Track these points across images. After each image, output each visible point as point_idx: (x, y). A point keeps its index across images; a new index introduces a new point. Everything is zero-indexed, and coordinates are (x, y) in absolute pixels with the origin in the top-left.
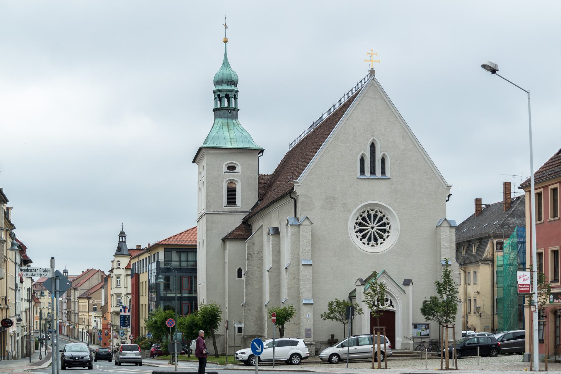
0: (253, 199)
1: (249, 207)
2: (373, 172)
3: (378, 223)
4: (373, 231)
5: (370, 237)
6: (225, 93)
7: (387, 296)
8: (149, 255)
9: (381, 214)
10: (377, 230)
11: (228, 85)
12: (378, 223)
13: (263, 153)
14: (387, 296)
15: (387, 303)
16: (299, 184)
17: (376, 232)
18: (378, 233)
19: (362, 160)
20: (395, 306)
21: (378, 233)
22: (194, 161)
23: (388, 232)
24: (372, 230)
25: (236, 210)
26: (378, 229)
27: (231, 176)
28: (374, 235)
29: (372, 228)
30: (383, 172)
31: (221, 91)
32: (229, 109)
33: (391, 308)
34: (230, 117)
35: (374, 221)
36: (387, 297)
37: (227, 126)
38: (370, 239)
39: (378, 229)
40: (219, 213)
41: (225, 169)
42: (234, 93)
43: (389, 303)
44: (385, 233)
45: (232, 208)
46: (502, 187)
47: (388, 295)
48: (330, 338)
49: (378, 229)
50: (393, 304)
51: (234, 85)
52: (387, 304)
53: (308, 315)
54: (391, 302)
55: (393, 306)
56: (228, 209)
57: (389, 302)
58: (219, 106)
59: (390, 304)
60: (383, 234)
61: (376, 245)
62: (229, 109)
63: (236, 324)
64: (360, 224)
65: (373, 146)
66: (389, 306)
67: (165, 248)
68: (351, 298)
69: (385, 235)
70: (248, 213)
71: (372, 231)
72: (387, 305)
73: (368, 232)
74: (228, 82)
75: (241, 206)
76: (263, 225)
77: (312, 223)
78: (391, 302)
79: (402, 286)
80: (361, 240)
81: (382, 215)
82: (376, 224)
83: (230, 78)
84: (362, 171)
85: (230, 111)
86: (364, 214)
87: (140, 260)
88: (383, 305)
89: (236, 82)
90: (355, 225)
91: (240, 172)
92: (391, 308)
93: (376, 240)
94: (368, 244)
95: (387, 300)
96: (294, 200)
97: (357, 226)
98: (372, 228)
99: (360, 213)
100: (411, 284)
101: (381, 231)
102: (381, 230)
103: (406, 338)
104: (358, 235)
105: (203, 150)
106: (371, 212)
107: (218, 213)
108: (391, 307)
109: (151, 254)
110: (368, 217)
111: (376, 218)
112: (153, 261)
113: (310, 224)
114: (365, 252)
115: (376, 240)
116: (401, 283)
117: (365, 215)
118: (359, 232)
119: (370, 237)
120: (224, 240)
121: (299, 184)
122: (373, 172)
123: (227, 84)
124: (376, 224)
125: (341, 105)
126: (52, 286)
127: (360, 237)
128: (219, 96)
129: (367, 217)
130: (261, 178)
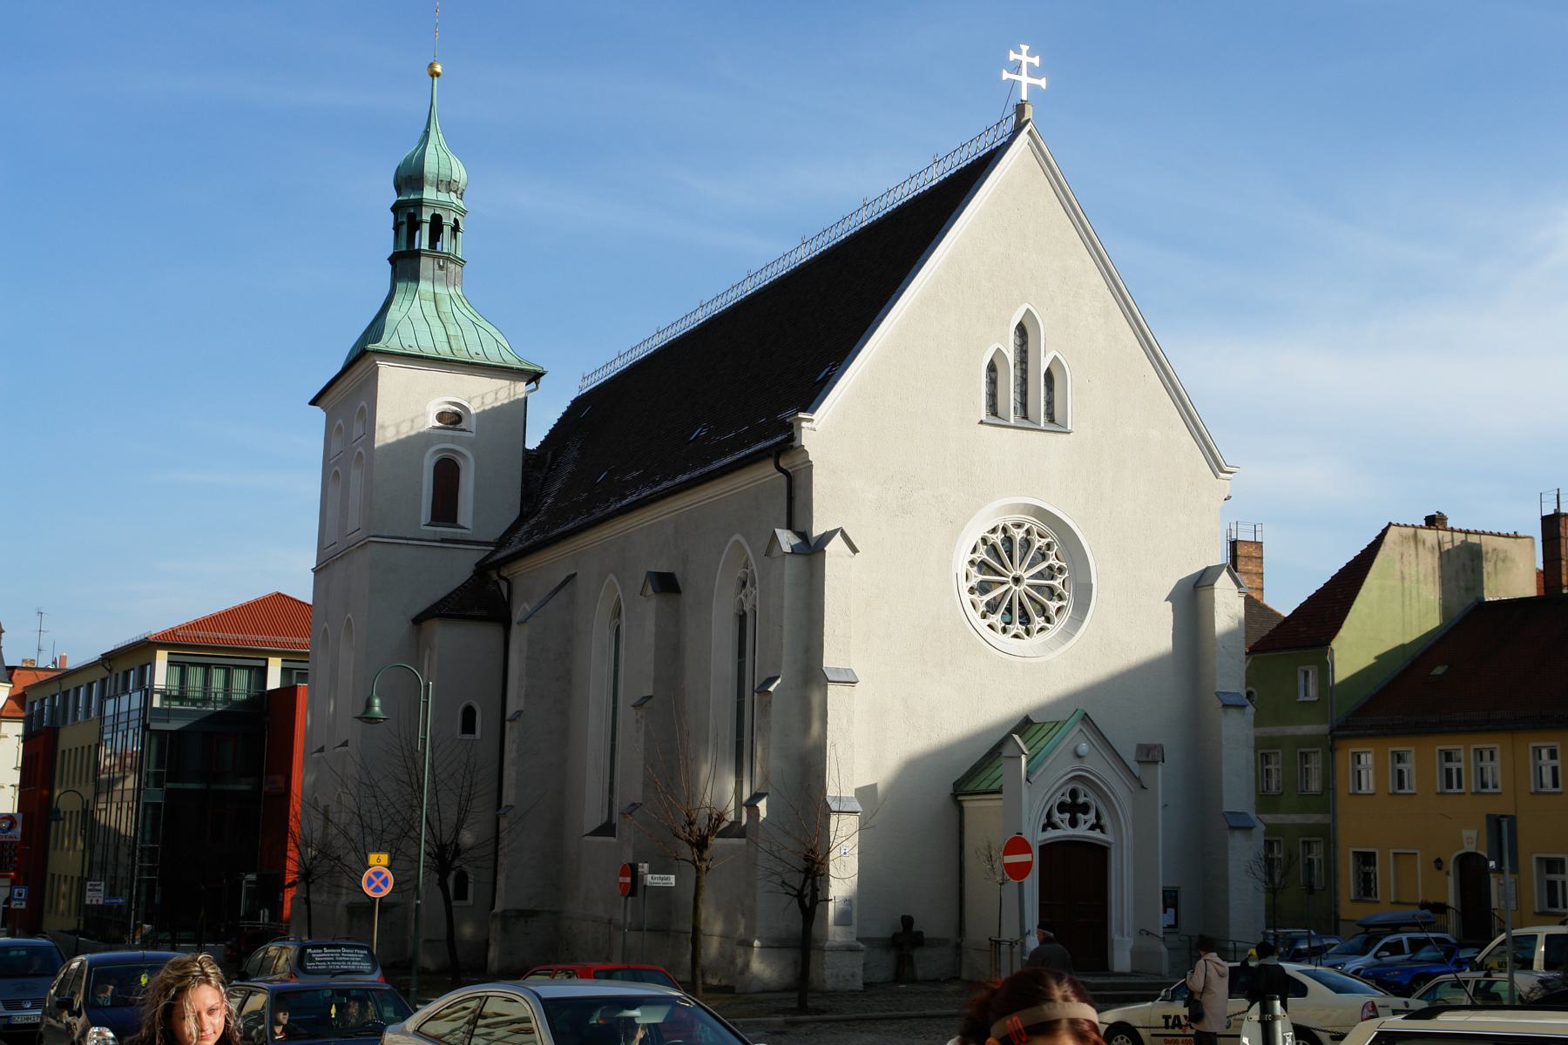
0: (508, 509)
1: (495, 531)
5: (1009, 610)
8: (106, 674)
9: (1043, 540)
13: (539, 385)
14: (1085, 796)
15: (1086, 817)
20: (1109, 828)
22: (314, 402)
24: (1014, 587)
25: (459, 537)
29: (1017, 580)
30: (1051, 417)
33: (1096, 834)
34: (440, 280)
36: (1087, 799)
37: (433, 304)
39: (1030, 586)
40: (405, 542)
43: (1091, 817)
45: (447, 531)
47: (1090, 793)
48: (900, 930)
50: (1102, 822)
51: (455, 192)
52: (1085, 822)
54: (1098, 817)
56: (435, 532)
58: (404, 249)
60: (1045, 601)
63: (649, 876)
64: (983, 566)
66: (1092, 828)
67: (169, 653)
68: (960, 798)
70: (492, 548)
72: (1088, 825)
74: (442, 181)
75: (470, 527)
76: (572, 577)
77: (854, 550)
78: (1098, 817)
85: (441, 264)
86: (1015, 530)
87: (64, 689)
88: (1073, 823)
89: (460, 186)
91: (473, 429)
92: (1097, 834)
95: (1085, 809)
96: (784, 476)
98: (1017, 580)
99: (1009, 520)
102: (1038, 588)
103: (1148, 934)
107: (410, 542)
108: (1098, 830)
109: (115, 671)
110: (1003, 545)
112: (112, 692)
116: (1130, 758)
117: (1018, 535)
119: (1009, 610)
120: (418, 621)
123: (437, 187)
125: (887, 209)
126: (1060, 538)
130: (526, 452)
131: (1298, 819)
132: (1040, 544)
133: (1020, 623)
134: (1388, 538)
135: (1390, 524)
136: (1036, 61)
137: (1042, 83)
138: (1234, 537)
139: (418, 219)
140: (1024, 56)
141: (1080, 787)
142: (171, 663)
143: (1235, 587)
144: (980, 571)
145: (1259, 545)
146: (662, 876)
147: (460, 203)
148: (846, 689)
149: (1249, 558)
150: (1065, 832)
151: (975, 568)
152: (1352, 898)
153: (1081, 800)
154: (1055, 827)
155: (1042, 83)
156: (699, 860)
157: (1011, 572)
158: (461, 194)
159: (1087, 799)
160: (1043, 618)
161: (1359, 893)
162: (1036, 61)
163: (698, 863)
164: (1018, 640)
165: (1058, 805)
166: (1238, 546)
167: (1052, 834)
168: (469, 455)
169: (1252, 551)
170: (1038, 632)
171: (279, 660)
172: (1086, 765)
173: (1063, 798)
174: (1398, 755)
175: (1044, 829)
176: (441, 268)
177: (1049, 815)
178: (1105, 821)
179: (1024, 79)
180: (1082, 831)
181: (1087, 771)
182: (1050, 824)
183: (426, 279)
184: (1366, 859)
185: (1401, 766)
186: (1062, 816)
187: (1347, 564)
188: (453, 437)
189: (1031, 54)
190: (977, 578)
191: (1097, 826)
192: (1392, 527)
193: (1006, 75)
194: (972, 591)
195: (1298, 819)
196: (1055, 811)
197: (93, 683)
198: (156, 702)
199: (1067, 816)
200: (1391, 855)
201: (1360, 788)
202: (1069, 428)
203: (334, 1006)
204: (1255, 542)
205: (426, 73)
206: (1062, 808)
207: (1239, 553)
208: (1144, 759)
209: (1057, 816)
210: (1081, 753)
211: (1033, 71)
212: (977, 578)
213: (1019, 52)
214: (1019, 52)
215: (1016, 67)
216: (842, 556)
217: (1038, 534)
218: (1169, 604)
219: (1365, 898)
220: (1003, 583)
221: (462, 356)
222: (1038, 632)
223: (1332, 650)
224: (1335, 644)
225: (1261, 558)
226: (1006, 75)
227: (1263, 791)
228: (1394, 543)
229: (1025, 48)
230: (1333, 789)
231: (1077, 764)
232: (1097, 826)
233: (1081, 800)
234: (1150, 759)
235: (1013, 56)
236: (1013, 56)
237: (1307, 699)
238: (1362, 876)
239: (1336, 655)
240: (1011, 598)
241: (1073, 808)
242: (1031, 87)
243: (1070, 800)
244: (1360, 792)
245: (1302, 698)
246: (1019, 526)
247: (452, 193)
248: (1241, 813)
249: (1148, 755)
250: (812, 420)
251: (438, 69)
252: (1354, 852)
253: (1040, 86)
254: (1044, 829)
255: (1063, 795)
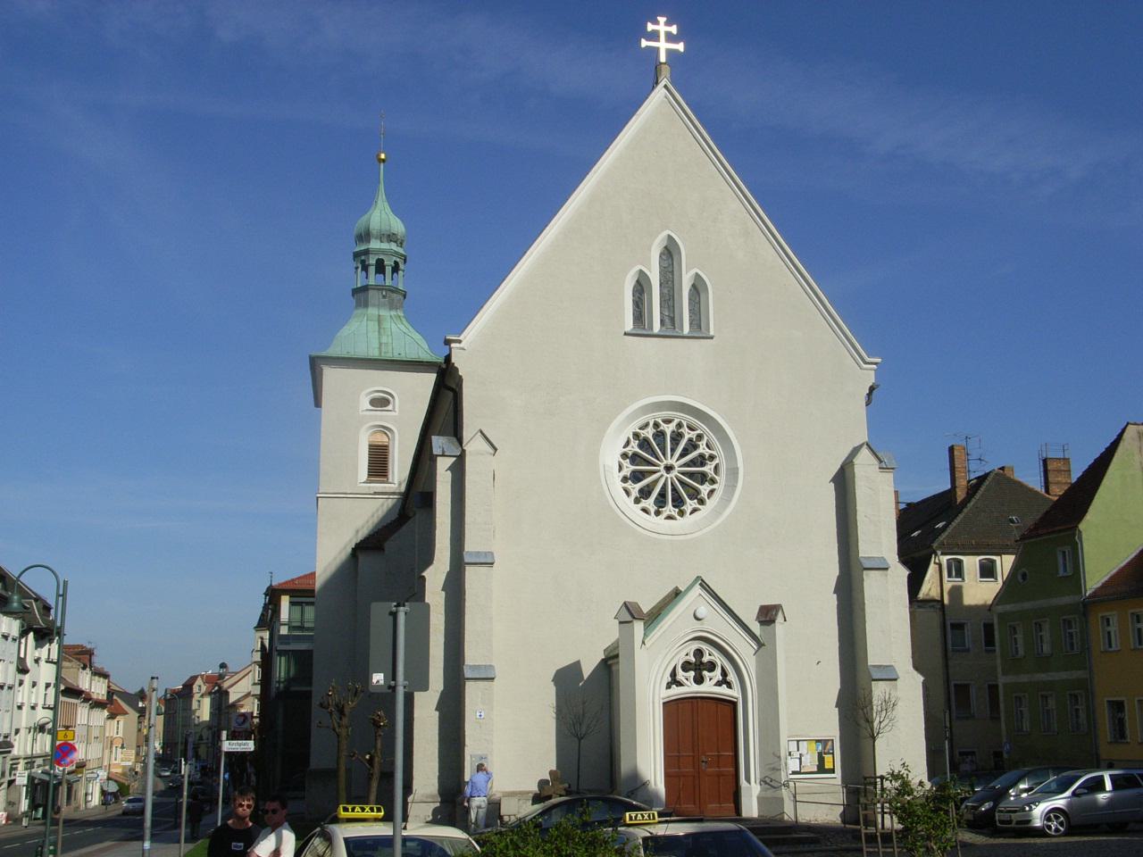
2: (670, 319)
3: (682, 456)
4: (671, 478)
5: (662, 495)
6: (377, 257)
7: (710, 655)
10: (683, 477)
11: (381, 242)
12: (682, 456)
14: (710, 655)
16: (461, 345)
17: (679, 480)
18: (682, 482)
19: (641, 287)
21: (682, 482)
23: (702, 502)
24: (666, 475)
26: (683, 474)
27: (382, 417)
28: (674, 489)
29: (669, 469)
31: (367, 252)
32: (383, 289)
33: (724, 690)
35: (673, 450)
37: (376, 323)
38: (661, 499)
41: (365, 404)
42: (394, 258)
43: (717, 674)
44: (702, 483)
46: (668, 589)
49: (683, 474)
51: (395, 242)
52: (710, 679)
53: (478, 714)
54: (724, 673)
55: (729, 685)
56: (369, 487)
57: (718, 671)
59: (721, 678)
61: (678, 517)
62: (383, 289)
64: (635, 459)
65: (670, 253)
66: (719, 684)
68: (610, 662)
69: (704, 489)
71: (662, 476)
72: (714, 681)
73: (656, 482)
78: (724, 673)
79: (756, 628)
80: (637, 501)
81: (693, 435)
82: (677, 460)
83: (388, 228)
84: (640, 316)
85: (384, 293)
88: (699, 680)
90: (621, 460)
92: (724, 690)
93: (678, 502)
94: (658, 513)
95: (711, 666)
97: (626, 463)
98: (669, 469)
100: (780, 618)
101: (691, 479)
102: (691, 475)
104: (630, 487)
105: (732, 706)
106: (665, 425)
108: (724, 686)
110: (654, 439)
111: (678, 444)
113: (492, 451)
114: (649, 534)
115: (678, 502)
118: (630, 479)
121: (461, 345)
122: (670, 319)
124: (677, 460)
127: (635, 493)
128: (363, 262)
129: (652, 440)
131: (1064, 675)
132: (690, 436)
133: (674, 506)
134: (1125, 435)
135: (1128, 424)
136: (674, 29)
137: (680, 47)
138: (1044, 456)
139: (367, 263)
140: (662, 26)
141: (704, 647)
142: (292, 604)
143: (876, 462)
144: (633, 462)
145: (1066, 461)
146: (240, 742)
147: (401, 250)
148: (483, 569)
149: (1059, 471)
150: (690, 688)
151: (628, 460)
152: (1109, 740)
153: (706, 659)
154: (680, 684)
155: (680, 47)
156: (339, 726)
157: (662, 461)
158: (401, 243)
159: (712, 658)
160: (696, 501)
161: (1115, 737)
162: (674, 29)
163: (337, 730)
164: (672, 521)
165: (683, 664)
166: (1048, 463)
167: (676, 692)
168: (395, 431)
169: (1060, 465)
170: (691, 514)
171: (288, 597)
172: (705, 627)
173: (688, 657)
174: (1138, 616)
175: (669, 686)
176: (384, 297)
177: (674, 674)
178: (732, 677)
179: (663, 46)
180: (709, 687)
181: (708, 632)
182: (674, 681)
183: (374, 305)
184: (1118, 706)
185: (1139, 626)
186: (686, 674)
187: (1095, 460)
188: (381, 416)
189: (668, 24)
190: (629, 468)
191: (724, 681)
192: (1130, 426)
193: (644, 43)
194: (625, 479)
195: (1064, 675)
196: (680, 671)
197: (759, 649)
198: (284, 631)
199: (692, 674)
200: (1136, 703)
201: (1110, 646)
202: (712, 333)
203: (920, 531)
204: (1064, 459)
205: (376, 161)
206: (686, 666)
207: (1049, 468)
208: (763, 619)
209: (681, 675)
210: (699, 616)
211: (670, 38)
212: (629, 468)
213: (657, 23)
214: (657, 23)
215: (654, 36)
216: (482, 454)
217: (688, 427)
218: (832, 485)
219: (1120, 741)
220: (655, 472)
221: (389, 356)
222: (691, 514)
223: (1080, 532)
224: (1082, 526)
225: (1070, 471)
226: (644, 43)
227: (1038, 654)
228: (1133, 439)
229: (662, 20)
230: (1088, 648)
231: (697, 625)
232: (724, 681)
233: (706, 659)
234: (768, 619)
235: (650, 27)
236: (650, 27)
237: (1065, 574)
238: (1117, 722)
239: (1084, 536)
240: (672, 484)
241: (698, 667)
242: (669, 52)
243: (694, 660)
244: (1110, 650)
245: (1061, 573)
246: (668, 421)
247: (393, 243)
248: (887, 666)
249: (766, 615)
250: (460, 342)
251: (383, 156)
252: (1108, 701)
253: (647, 40)
254: (669, 686)
255: (687, 655)
